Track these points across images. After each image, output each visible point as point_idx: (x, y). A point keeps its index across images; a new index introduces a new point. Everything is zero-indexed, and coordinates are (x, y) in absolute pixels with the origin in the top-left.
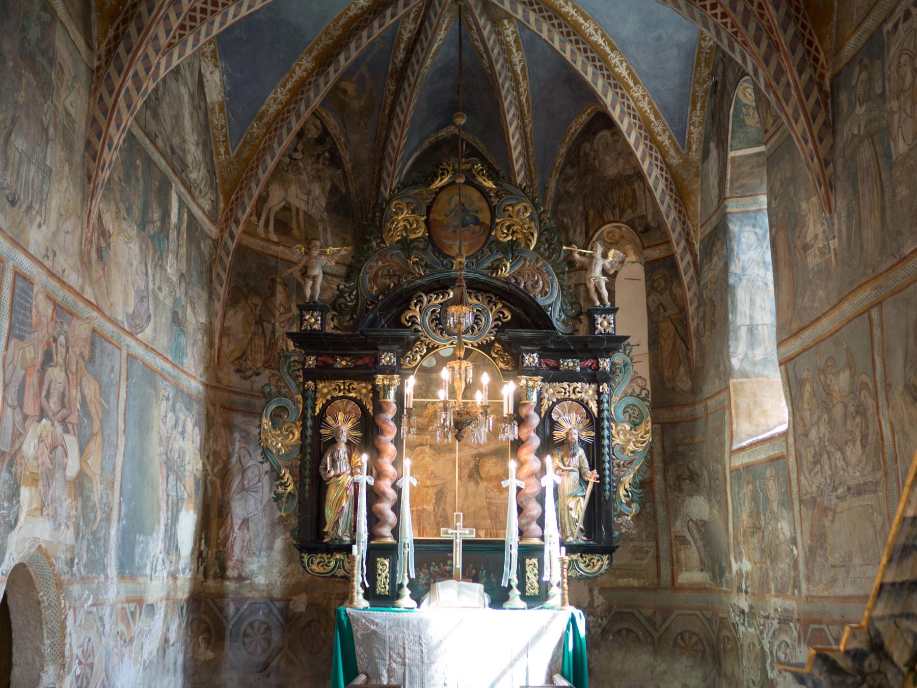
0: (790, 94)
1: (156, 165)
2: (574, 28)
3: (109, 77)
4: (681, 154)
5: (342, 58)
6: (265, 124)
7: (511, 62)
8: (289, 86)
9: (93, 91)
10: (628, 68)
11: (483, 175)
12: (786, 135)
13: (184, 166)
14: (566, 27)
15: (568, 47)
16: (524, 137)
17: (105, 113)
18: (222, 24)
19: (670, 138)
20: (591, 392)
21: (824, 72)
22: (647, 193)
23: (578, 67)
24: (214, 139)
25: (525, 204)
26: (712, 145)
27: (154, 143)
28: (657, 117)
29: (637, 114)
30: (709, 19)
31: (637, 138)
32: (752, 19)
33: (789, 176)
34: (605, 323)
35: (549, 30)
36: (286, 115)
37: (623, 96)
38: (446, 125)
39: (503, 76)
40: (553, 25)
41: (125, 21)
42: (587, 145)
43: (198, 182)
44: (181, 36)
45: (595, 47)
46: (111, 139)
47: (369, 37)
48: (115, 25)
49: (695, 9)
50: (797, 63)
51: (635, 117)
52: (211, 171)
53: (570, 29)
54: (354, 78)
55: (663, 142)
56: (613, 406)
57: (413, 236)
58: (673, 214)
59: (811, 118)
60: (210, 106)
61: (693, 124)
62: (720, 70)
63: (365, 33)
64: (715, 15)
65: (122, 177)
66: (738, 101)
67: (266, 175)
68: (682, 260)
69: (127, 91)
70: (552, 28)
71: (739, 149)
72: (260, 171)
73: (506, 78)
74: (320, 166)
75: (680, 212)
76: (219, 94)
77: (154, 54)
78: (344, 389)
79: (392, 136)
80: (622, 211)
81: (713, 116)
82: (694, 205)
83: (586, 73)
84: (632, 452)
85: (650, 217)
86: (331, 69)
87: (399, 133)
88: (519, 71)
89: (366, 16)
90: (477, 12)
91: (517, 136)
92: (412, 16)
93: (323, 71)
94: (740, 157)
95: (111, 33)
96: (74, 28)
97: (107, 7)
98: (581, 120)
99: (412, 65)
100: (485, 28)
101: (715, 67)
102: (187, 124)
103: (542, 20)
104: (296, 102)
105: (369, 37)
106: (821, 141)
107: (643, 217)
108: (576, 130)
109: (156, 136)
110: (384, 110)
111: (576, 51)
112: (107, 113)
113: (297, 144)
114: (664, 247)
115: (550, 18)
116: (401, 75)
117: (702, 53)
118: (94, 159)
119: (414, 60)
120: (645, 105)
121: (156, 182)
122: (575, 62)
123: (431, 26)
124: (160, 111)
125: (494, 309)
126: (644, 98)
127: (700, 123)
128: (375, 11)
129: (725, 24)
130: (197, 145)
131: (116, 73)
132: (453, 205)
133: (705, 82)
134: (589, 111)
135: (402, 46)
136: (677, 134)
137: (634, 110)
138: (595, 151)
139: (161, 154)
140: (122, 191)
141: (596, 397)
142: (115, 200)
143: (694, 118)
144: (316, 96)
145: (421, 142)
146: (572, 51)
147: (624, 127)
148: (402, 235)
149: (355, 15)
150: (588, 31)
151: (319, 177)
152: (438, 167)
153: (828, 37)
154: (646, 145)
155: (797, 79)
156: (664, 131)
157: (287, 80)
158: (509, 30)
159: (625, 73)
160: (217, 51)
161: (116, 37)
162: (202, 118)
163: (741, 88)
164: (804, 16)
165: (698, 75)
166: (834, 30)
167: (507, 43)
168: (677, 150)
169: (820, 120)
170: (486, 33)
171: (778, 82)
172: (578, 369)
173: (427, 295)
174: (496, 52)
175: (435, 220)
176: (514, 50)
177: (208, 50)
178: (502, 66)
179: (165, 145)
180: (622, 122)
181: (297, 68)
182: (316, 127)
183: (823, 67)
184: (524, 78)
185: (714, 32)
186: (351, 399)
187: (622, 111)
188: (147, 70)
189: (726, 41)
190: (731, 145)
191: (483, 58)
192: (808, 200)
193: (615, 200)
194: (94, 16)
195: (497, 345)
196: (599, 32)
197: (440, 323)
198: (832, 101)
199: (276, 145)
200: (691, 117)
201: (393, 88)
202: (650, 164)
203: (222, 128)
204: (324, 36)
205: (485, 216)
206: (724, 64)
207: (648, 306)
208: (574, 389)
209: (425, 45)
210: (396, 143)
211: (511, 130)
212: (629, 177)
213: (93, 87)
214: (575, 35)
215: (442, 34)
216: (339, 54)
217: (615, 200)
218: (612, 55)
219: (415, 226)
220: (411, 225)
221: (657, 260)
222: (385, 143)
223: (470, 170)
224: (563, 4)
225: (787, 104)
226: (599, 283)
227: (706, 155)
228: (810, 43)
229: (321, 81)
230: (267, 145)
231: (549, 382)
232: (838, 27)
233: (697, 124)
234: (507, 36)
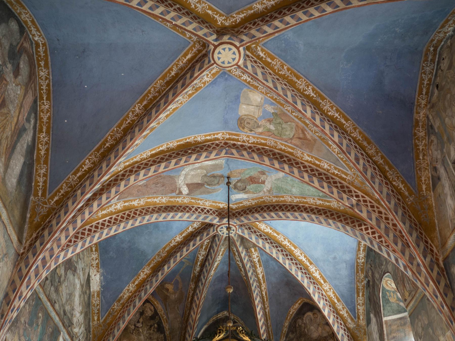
0: (421, 270)
1: (52, 318)
2: (289, 252)
3: (28, 258)
5: (166, 267)
6: (121, 304)
7: (256, 273)
8: (137, 283)
9: (16, 265)
10: (320, 274)
11: (243, 333)
12: (422, 295)
13: (71, 324)
14: (285, 252)
15: (287, 262)
16: (265, 314)
17: (20, 278)
18: (99, 238)
19: (347, 312)
21: (438, 257)
23: (293, 272)
24: (92, 312)
26: (372, 316)
27: (53, 306)
28: (339, 301)
29: (327, 299)
30: (365, 236)
31: (329, 312)
32: (390, 231)
33: (426, 322)
35: (276, 253)
36: (133, 299)
37: (318, 289)
38: (222, 311)
39: (252, 279)
40: (278, 250)
41: (43, 229)
42: (300, 321)
43: (79, 335)
44: (75, 242)
45: (301, 263)
46: (21, 293)
47: (181, 256)
48: (37, 232)
49: (356, 231)
50: (421, 252)
51: (326, 300)
52: (88, 329)
53: (288, 253)
55: (343, 315)
59: (437, 283)
60: (92, 294)
61: (359, 304)
62: (370, 274)
63: (178, 254)
64: (368, 233)
65: (27, 321)
66: (384, 289)
67: (118, 333)
69: (37, 267)
70: (278, 252)
71: (389, 316)
72: (116, 330)
73: (254, 280)
74: (152, 331)
76: (98, 286)
77: (57, 248)
79: (192, 313)
81: (370, 300)
83: (298, 276)
86: (160, 273)
87: (196, 311)
88: (261, 278)
89: (180, 246)
90: (238, 244)
91: (261, 313)
92: (204, 247)
93: (155, 275)
94: (390, 320)
95: (34, 235)
96: (11, 228)
97: (35, 222)
98: (295, 307)
99: (204, 273)
100: (242, 253)
101: (367, 273)
102: (77, 300)
103: (272, 247)
104: (139, 292)
105: (181, 256)
106: (446, 295)
108: (293, 313)
109: (55, 302)
110: (188, 299)
111: (291, 264)
112: (22, 278)
113: (140, 318)
115: (277, 247)
116: (198, 279)
117: (359, 266)
118: (8, 304)
119: (204, 270)
120: (331, 294)
121: (50, 329)
122: (291, 270)
123: (214, 251)
124: (61, 289)
126: (330, 290)
127: (363, 304)
128: (185, 243)
129: (375, 237)
130: (81, 313)
131: (32, 256)
133: (362, 281)
134: (299, 302)
135: (199, 264)
136: (351, 310)
137: (325, 296)
138: (304, 324)
139: (57, 313)
140: (25, 330)
142: (19, 334)
144: (150, 288)
145: (208, 320)
146: (289, 264)
147: (321, 306)
149: (174, 245)
150: (297, 254)
151: (151, 338)
152: (217, 329)
153: (435, 239)
154: (334, 316)
155: (424, 261)
156: (343, 308)
157: (136, 280)
158: (255, 255)
160: (100, 264)
161: (36, 238)
162: (86, 299)
163: (385, 281)
164: (420, 228)
165: (358, 278)
166: (438, 235)
167: (254, 262)
168: (352, 319)
169: (443, 283)
170: (243, 255)
171: (412, 264)
174: (248, 266)
176: (258, 266)
177: (95, 263)
178: (252, 274)
179: (60, 309)
181: (142, 273)
182: (151, 310)
183: (436, 254)
184: (264, 282)
185: (369, 242)
187: (319, 297)
188: (51, 257)
189: (376, 246)
190: (384, 314)
191: (241, 270)
192: (444, 335)
194: (26, 226)
196: (303, 255)
198: (447, 273)
199: (126, 315)
200: (357, 300)
201: (193, 287)
202: (338, 327)
203: (97, 306)
204: (157, 256)
206: (372, 270)
209: (211, 262)
210: (194, 317)
211: (258, 310)
213: (17, 263)
214: (290, 256)
215: (219, 258)
216: (164, 265)
218: (311, 267)
222: (188, 316)
223: (236, 331)
224: (283, 240)
225: (420, 276)
227: (369, 322)
228: (427, 242)
229: (154, 280)
230: (121, 315)
232: (440, 233)
233: (361, 304)
234: (254, 258)
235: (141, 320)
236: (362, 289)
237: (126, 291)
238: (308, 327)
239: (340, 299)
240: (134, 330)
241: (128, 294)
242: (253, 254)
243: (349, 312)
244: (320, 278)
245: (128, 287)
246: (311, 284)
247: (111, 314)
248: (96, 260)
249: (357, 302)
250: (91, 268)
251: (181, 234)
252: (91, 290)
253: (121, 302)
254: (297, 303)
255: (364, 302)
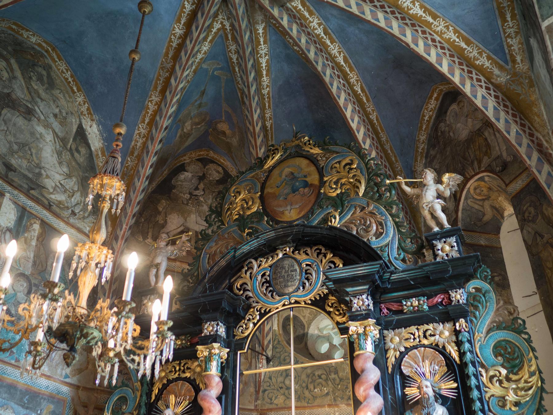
4: (506, 70)
6: (136, 157)
10: (421, 7)
19: (489, 58)
20: (447, 333)
22: (497, 135)
25: (350, 158)
28: (468, 43)
29: (446, 45)
31: (449, 65)
34: (447, 248)
37: (424, 32)
54: (224, 118)
56: (478, 346)
57: (249, 213)
58: (514, 129)
60: (94, 153)
61: (509, 36)
68: (540, 172)
73: (324, 65)
75: (523, 125)
76: (100, 141)
78: (180, 369)
80: (480, 162)
82: (538, 116)
83: (378, 20)
84: (517, 404)
85: (505, 154)
87: (169, 101)
88: (342, 63)
107: (499, 157)
108: (430, 117)
114: (524, 175)
120: (451, 35)
125: (324, 261)
126: (448, 29)
127: (517, 33)
132: (284, 177)
134: (435, 95)
138: (448, 126)
141: (454, 338)
143: (508, 31)
148: (239, 214)
149: (178, 45)
156: (480, 54)
157: (145, 116)
159: (420, 12)
160: (91, 108)
168: (501, 68)
172: (425, 307)
173: (256, 260)
174: (303, 41)
175: (268, 193)
176: (328, 42)
177: (84, 109)
180: (429, 55)
181: (150, 104)
186: (186, 379)
187: (426, 45)
190: (542, 16)
193: (472, 156)
195: (331, 297)
197: (270, 286)
199: (140, 169)
200: (504, 30)
202: (472, 85)
205: (314, 178)
207: (524, 240)
208: (425, 332)
211: (348, 114)
212: (479, 130)
217: (472, 156)
219: (250, 203)
220: (247, 204)
221: (522, 190)
226: (432, 207)
231: (393, 329)
233: (513, 35)
235: (201, 186)
236: (508, 6)
237: (138, 137)
238: (454, 126)
239: (470, 38)
240: (190, 199)
241: (140, 140)
242: (310, 22)
243: (494, 57)
244: (424, 15)
245: (139, 130)
246: (406, 28)
247: (126, 174)
248: (84, 104)
249: (505, 33)
250: (82, 117)
251: (179, 21)
252: (93, 149)
253: (135, 155)
254: (431, 97)
255: (518, 28)
